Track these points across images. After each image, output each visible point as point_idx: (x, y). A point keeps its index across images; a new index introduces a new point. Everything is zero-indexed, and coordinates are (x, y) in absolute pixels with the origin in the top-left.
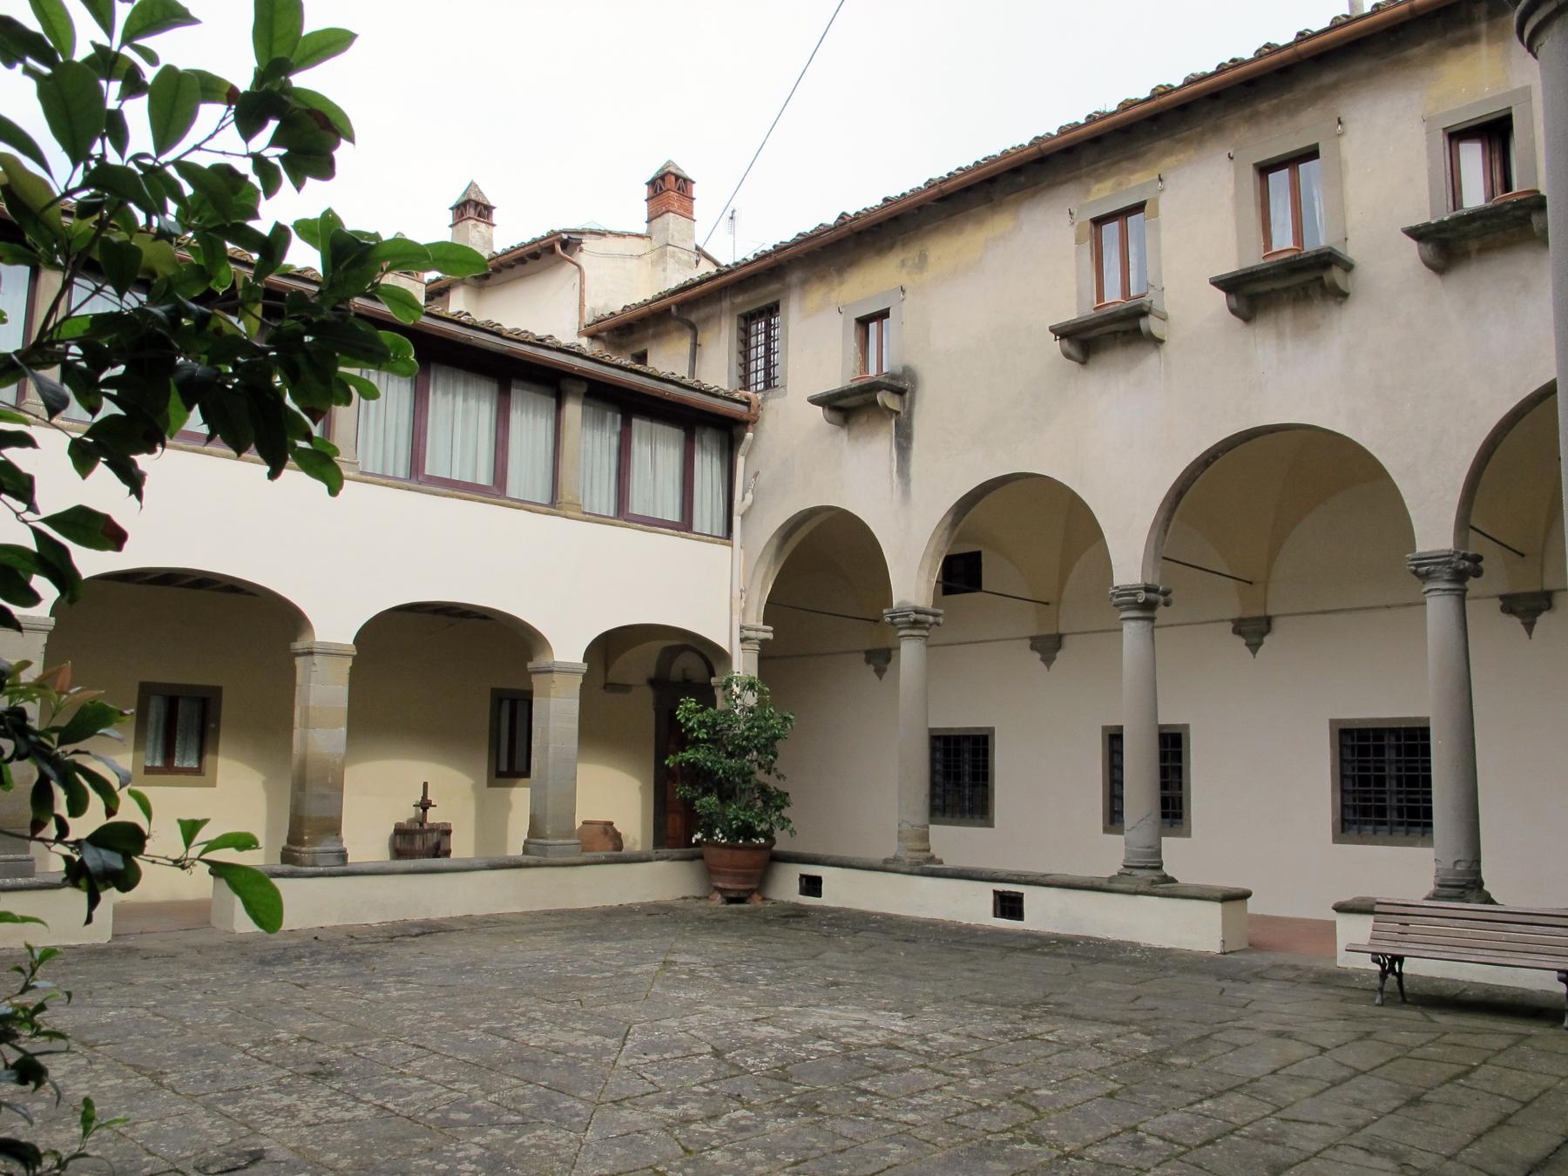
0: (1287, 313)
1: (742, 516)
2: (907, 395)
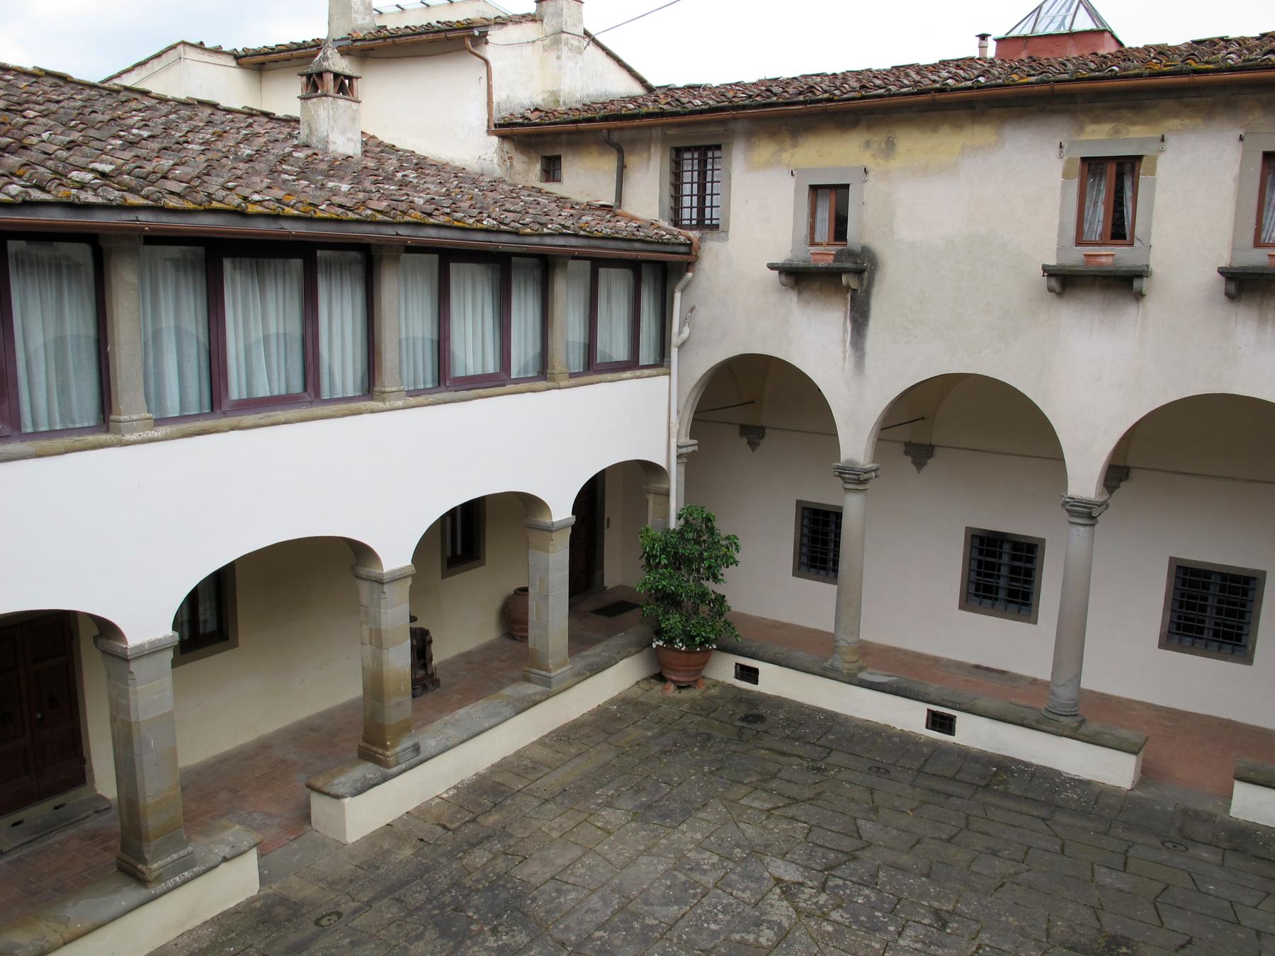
2: (866, 275)
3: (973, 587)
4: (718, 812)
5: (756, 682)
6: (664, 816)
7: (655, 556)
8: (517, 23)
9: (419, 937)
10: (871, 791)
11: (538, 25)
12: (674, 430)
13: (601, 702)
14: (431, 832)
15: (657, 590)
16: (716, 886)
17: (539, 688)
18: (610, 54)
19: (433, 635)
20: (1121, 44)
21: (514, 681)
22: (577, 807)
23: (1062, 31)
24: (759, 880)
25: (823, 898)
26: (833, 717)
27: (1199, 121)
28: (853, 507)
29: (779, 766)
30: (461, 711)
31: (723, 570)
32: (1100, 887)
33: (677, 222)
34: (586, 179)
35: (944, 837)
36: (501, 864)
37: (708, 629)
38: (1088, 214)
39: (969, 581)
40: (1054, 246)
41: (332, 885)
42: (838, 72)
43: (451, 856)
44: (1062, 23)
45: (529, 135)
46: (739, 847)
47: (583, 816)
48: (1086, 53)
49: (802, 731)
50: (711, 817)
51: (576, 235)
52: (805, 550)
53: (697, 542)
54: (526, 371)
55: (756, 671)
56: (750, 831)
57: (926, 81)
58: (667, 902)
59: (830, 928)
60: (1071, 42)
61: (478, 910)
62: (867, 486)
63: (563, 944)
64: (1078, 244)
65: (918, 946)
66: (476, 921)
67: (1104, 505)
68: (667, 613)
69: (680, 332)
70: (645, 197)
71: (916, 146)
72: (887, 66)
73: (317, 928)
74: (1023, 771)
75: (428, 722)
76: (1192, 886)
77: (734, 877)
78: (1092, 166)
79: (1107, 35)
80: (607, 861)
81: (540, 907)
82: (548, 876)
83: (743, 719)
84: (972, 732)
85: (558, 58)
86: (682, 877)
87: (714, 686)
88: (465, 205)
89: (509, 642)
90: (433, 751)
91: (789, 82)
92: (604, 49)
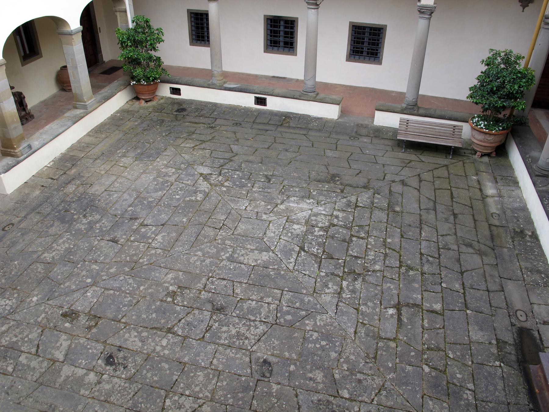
4: (172, 151)
5: (180, 94)
6: (149, 157)
7: (125, 42)
9: (52, 226)
10: (235, 133)
13: (112, 113)
14: (46, 182)
15: (128, 58)
16: (176, 181)
17: (82, 111)
19: (25, 94)
21: (69, 109)
22: (110, 160)
25: (220, 178)
26: (215, 105)
29: (195, 129)
30: (47, 127)
32: (327, 157)
36: (81, 189)
37: (155, 73)
39: (267, 40)
41: (5, 213)
43: (58, 190)
47: (113, 163)
50: (169, 154)
52: (194, 33)
53: (144, 33)
55: (179, 90)
56: (187, 157)
58: (156, 191)
59: (225, 189)
61: (75, 210)
63: (116, 216)
65: (260, 190)
66: (76, 214)
68: (135, 68)
73: (3, 232)
74: (295, 117)
75: (32, 135)
77: (183, 176)
80: (127, 180)
81: (102, 203)
82: (103, 190)
83: (176, 111)
84: (274, 104)
86: (161, 180)
90: (38, 147)
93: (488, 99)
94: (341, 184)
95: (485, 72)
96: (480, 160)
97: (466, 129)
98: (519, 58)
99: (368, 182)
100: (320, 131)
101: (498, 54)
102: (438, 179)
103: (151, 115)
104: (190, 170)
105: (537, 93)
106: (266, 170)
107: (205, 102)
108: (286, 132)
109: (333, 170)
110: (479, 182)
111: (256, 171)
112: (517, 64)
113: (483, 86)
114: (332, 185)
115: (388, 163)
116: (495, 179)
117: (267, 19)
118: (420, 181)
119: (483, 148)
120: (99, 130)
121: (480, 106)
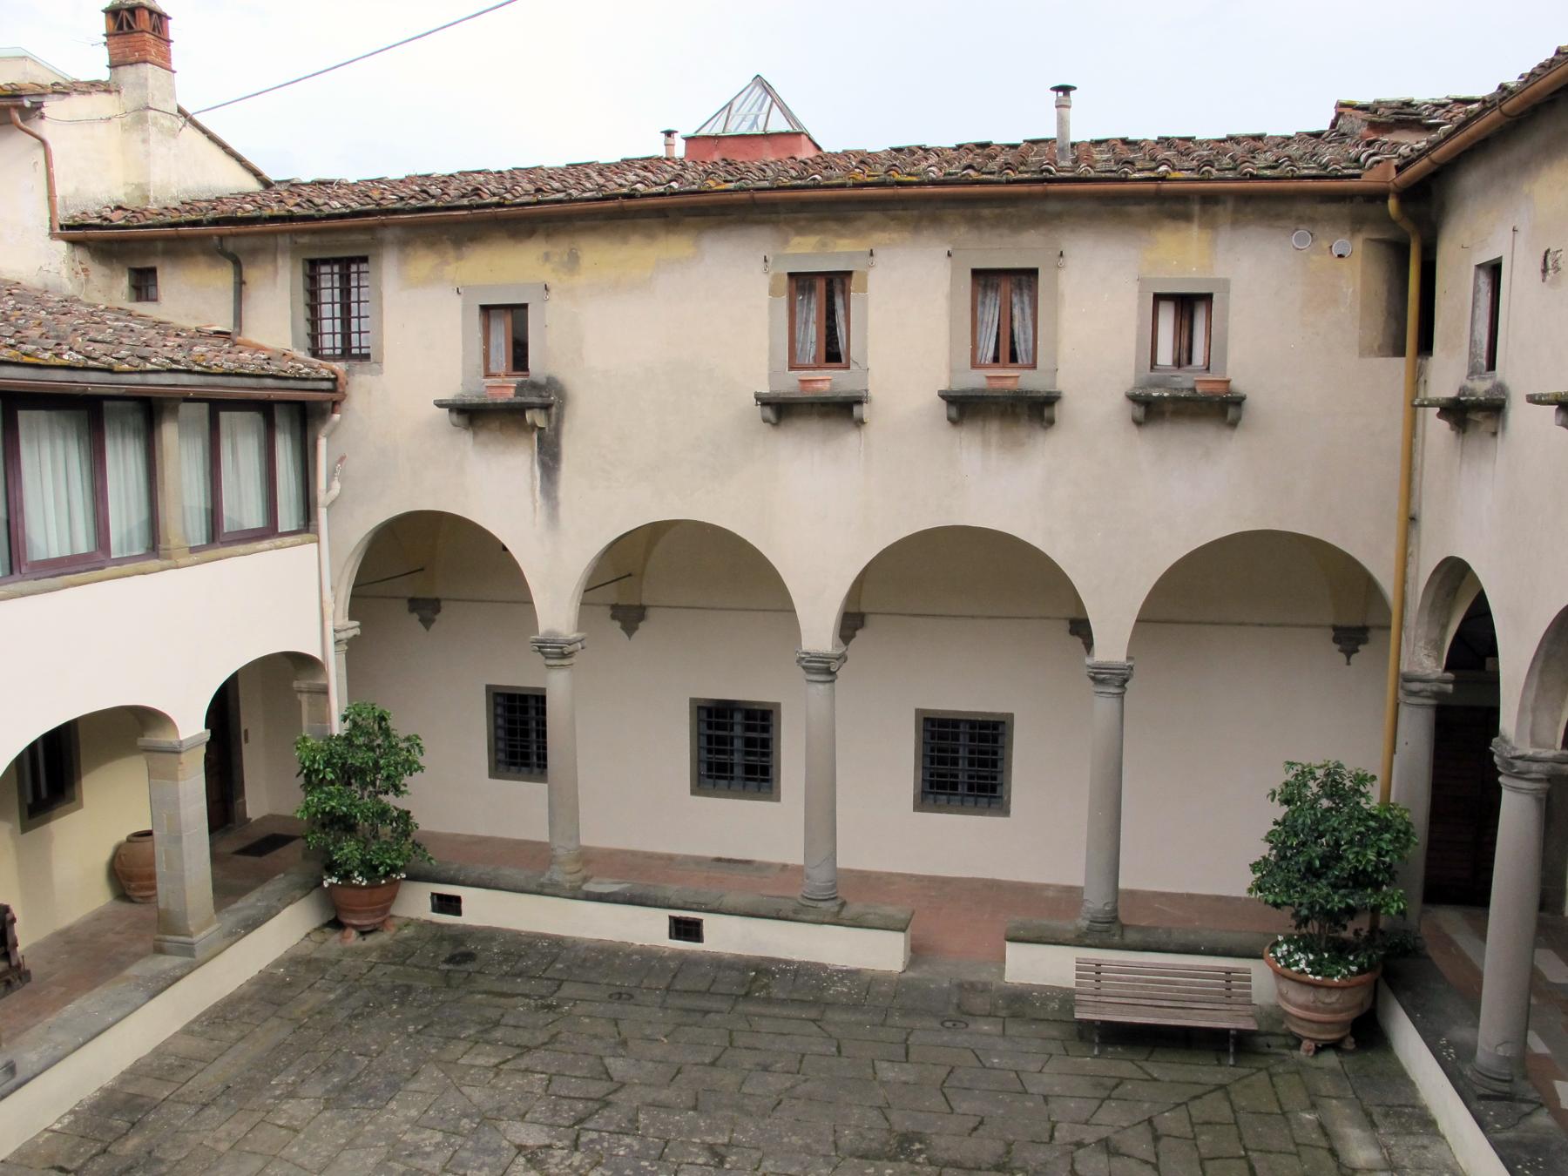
0: (994, 427)
1: (329, 507)
2: (554, 410)
3: (704, 767)
5: (458, 912)
6: (365, 1097)
7: (317, 771)
8: (84, 93)
11: (114, 96)
12: (329, 611)
13: (262, 967)
15: (324, 812)
18: (212, 138)
20: (819, 148)
21: (138, 956)
23: (755, 131)
24: (496, 1152)
25: (577, 1158)
26: (558, 942)
27: (906, 235)
28: (558, 687)
29: (501, 1011)
30: (71, 1007)
31: (406, 779)
32: (883, 1084)
33: (315, 352)
34: (191, 299)
35: (707, 1060)
37: (394, 855)
38: (799, 335)
39: (699, 761)
40: (765, 371)
42: (504, 168)
44: (755, 122)
45: (109, 241)
46: (466, 1116)
47: (257, 1116)
48: (784, 156)
49: (523, 964)
51: (189, 372)
52: (501, 745)
54: (130, 547)
55: (458, 899)
56: (477, 1095)
57: (612, 186)
60: (766, 144)
62: (573, 660)
64: (791, 368)
67: (842, 658)
69: (329, 488)
70: (276, 321)
71: (603, 258)
72: (562, 163)
76: (977, 1064)
77: (464, 1154)
78: (801, 282)
79: (804, 137)
84: (726, 936)
85: (145, 141)
87: (407, 925)
88: (35, 333)
89: (125, 907)
90: (36, 1068)
91: (447, 180)
92: (204, 131)
93: (1303, 891)
94: (930, 1162)
95: (1284, 820)
96: (1313, 1062)
97: (1261, 979)
98: (1362, 779)
99: (1008, 1153)
100: (855, 1006)
101: (1306, 774)
102: (1205, 1128)
103: (377, 973)
104: (487, 1137)
105: (1430, 860)
106: (709, 1132)
107: (528, 935)
108: (761, 1016)
109: (903, 1122)
110: (1322, 1128)
111: (680, 1133)
112: (1363, 795)
113: (1284, 858)
114: (905, 1165)
115: (1057, 1090)
116: (1368, 1115)
117: (699, 708)
118: (1156, 1138)
119: (1315, 1027)
120: (222, 1015)
121: (1288, 911)
